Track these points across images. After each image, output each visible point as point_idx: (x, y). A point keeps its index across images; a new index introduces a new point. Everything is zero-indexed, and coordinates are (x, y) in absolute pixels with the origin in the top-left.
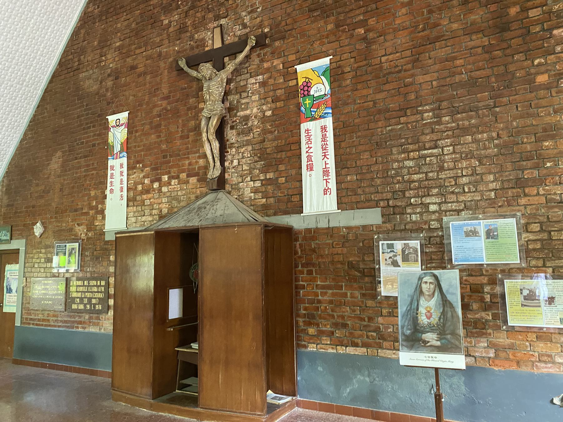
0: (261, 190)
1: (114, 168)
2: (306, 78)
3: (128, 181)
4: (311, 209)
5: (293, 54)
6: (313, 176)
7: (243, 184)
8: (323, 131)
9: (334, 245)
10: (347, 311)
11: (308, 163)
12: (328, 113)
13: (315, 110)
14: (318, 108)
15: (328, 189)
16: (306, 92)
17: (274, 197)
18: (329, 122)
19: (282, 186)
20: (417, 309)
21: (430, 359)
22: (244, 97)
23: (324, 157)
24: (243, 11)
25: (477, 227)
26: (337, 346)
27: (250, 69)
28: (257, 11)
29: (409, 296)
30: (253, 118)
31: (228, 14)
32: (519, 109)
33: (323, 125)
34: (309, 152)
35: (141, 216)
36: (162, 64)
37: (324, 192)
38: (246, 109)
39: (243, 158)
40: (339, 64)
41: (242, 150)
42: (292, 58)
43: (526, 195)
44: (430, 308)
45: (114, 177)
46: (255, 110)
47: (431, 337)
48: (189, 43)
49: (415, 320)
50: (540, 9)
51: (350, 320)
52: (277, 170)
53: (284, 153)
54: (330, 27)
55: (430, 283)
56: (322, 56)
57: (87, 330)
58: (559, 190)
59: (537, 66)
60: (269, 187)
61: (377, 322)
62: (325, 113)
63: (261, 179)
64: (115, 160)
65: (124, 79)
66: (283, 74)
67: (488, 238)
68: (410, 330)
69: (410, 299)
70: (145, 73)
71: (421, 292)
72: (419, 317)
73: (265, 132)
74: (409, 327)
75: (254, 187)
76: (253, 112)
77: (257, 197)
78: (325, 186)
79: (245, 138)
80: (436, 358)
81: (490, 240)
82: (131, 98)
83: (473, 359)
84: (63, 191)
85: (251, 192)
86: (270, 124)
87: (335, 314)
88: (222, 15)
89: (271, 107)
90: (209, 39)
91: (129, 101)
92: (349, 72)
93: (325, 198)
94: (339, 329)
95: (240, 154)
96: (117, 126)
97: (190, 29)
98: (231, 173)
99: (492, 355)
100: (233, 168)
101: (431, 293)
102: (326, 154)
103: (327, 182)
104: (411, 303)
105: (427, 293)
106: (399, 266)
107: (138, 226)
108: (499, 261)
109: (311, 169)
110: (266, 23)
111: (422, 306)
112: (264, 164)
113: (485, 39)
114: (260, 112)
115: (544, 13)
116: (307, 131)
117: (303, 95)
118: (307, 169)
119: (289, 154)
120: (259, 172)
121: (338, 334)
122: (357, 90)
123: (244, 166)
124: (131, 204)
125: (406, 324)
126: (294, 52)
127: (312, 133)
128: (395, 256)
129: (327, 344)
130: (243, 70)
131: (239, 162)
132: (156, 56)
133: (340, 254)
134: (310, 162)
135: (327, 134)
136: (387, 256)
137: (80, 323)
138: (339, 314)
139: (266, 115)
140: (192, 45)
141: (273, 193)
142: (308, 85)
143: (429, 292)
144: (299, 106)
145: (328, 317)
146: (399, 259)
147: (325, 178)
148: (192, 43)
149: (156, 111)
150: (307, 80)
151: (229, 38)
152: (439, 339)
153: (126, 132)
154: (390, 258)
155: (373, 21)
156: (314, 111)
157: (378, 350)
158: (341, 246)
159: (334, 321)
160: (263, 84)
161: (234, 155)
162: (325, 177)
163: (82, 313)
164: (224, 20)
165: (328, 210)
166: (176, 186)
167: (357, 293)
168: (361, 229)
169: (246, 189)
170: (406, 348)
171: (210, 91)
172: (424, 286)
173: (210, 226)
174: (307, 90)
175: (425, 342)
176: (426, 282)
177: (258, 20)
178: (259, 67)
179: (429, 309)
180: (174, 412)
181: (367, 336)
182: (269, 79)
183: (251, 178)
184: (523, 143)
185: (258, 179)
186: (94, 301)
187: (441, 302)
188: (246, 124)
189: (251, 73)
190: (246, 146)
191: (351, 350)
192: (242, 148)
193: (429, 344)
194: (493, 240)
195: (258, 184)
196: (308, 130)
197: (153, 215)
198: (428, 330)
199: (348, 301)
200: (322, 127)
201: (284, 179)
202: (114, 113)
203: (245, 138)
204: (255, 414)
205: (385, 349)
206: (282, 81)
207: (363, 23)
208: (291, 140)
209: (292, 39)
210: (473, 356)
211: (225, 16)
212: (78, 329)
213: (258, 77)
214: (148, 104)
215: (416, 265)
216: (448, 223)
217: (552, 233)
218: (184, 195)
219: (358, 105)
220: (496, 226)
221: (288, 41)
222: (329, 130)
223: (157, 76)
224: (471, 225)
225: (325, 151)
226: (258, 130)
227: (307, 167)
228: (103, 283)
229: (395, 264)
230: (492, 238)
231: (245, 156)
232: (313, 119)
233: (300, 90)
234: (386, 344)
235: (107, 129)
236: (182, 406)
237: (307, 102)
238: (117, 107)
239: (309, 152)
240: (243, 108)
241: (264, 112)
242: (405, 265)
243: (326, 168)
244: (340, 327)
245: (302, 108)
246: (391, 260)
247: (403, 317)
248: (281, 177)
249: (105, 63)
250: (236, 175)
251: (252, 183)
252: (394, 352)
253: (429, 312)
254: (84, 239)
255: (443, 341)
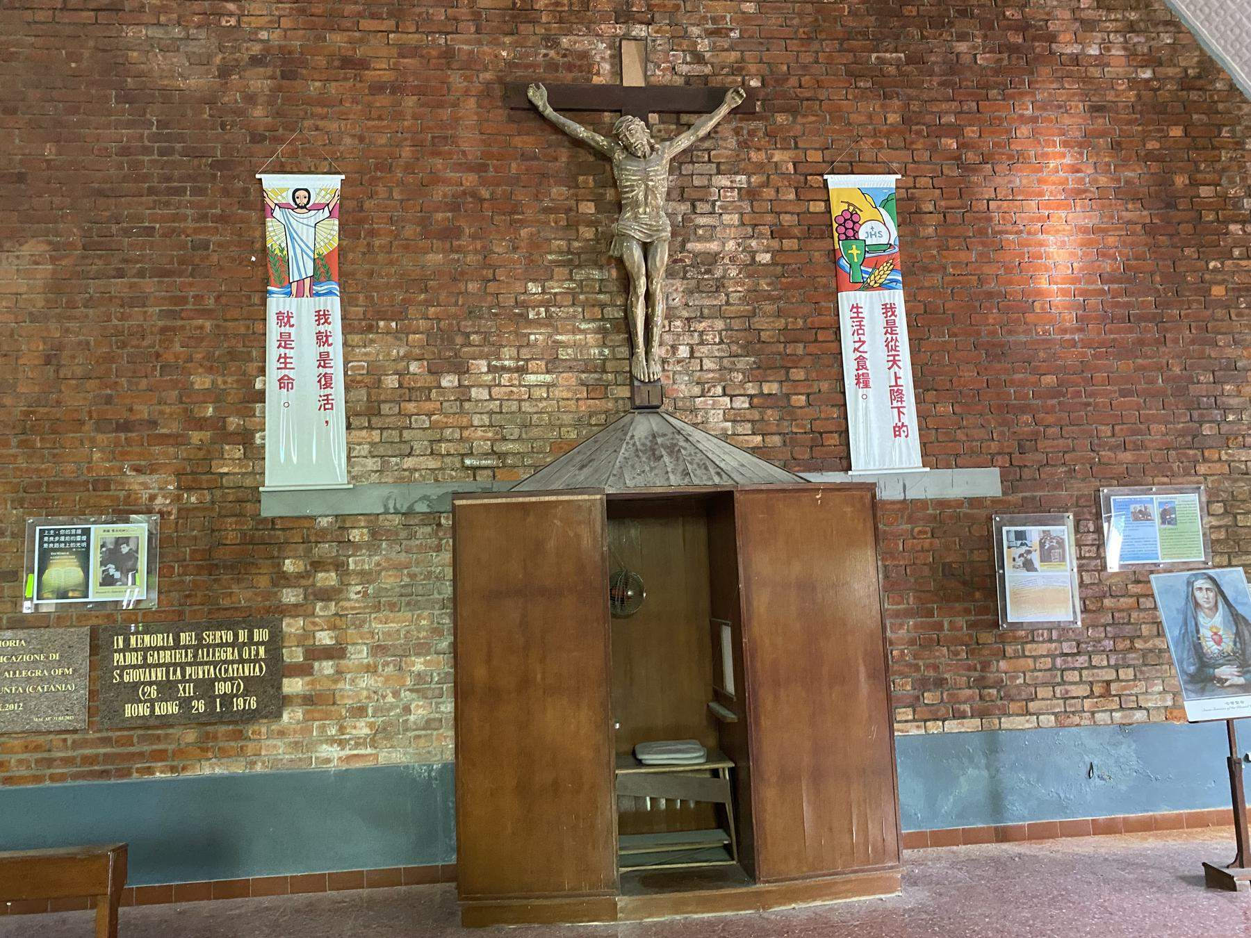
0: (749, 417)
1: (292, 321)
2: (850, 204)
3: (346, 363)
4: (867, 463)
5: (816, 149)
6: (871, 399)
7: (705, 402)
8: (889, 314)
9: (915, 534)
10: (944, 656)
11: (860, 372)
12: (897, 281)
13: (870, 270)
14: (876, 267)
15: (903, 425)
16: (850, 233)
17: (780, 434)
18: (897, 297)
19: (799, 411)
20: (1198, 631)
21: (1235, 705)
22: (702, 211)
23: (891, 363)
24: (693, 25)
25: (1149, 506)
26: (925, 721)
27: (716, 156)
28: (727, 36)
29: (1178, 610)
30: (727, 261)
31: (653, 17)
32: (1193, 331)
33: (887, 302)
34: (860, 349)
35: (402, 456)
36: (456, 79)
37: (895, 431)
38: (710, 239)
39: (702, 343)
40: (912, 193)
41: (702, 326)
42: (814, 156)
43: (1205, 460)
44: (1216, 628)
45: (294, 344)
46: (731, 245)
47: (1228, 672)
48: (544, 51)
49: (1198, 648)
50: (1212, 188)
51: (949, 671)
52: (788, 379)
53: (801, 346)
54: (893, 118)
55: (1207, 589)
56: (880, 170)
57: (188, 774)
58: (1243, 455)
59: (1212, 271)
60: (769, 412)
61: (997, 671)
62: (892, 281)
63: (749, 392)
64: (294, 299)
65: (318, 84)
66: (796, 185)
67: (1163, 523)
68: (1194, 665)
69: (1181, 617)
70: (396, 89)
71: (1197, 605)
72: (1204, 644)
73: (754, 295)
74: (1191, 660)
75: (732, 408)
76: (727, 249)
77: (740, 430)
78: (897, 421)
79: (707, 302)
80: (1242, 702)
81: (1167, 526)
82: (348, 141)
83: (1145, 712)
84: (59, 366)
85: (726, 421)
86: (768, 280)
87: (921, 663)
88: (637, 15)
89: (768, 246)
90: (602, 58)
91: (342, 148)
92: (931, 213)
93: (897, 444)
94: (929, 690)
95: (696, 334)
96: (299, 207)
97: (544, 19)
98: (671, 373)
99: (1169, 703)
100: (679, 362)
101: (1212, 604)
102: (897, 358)
103: (899, 412)
104: (1185, 623)
105: (1207, 606)
106: (1036, 570)
107: (391, 480)
108: (1178, 558)
109: (866, 385)
110: (753, 68)
111: (1203, 626)
112: (754, 362)
113: (1145, 213)
114: (743, 251)
115: (1217, 195)
116: (856, 308)
117: (843, 237)
118: (858, 383)
119: (813, 348)
120: (744, 377)
121: (929, 697)
122: (947, 249)
123: (705, 361)
124: (355, 422)
125: (1185, 656)
126: (817, 146)
127: (865, 313)
128: (1029, 552)
129: (906, 721)
130: (700, 153)
131: (692, 352)
132: (434, 53)
133: (928, 551)
134: (864, 371)
135: (897, 320)
136: (1017, 552)
137: (160, 755)
138: (928, 661)
139: (757, 259)
140: (552, 59)
141: (778, 425)
142: (851, 221)
143: (1209, 603)
144: (834, 256)
145: (906, 670)
146: (1035, 557)
147: (895, 404)
148: (552, 53)
149: (439, 193)
150: (851, 209)
151: (658, 73)
152: (1242, 674)
153: (337, 228)
154: (1021, 555)
155: (973, 132)
156: (866, 272)
157: (1000, 719)
158: (929, 535)
159: (919, 676)
160: (750, 194)
161: (680, 335)
162: (895, 402)
163: (172, 726)
164: (644, 27)
165: (904, 466)
166: (514, 389)
167: (961, 621)
168: (966, 505)
169: (713, 412)
170: (1193, 695)
171: (651, 183)
172: (1198, 594)
173: (763, 487)
174: (853, 229)
175: (1222, 681)
176: (1200, 589)
177: (733, 56)
178: (738, 155)
179: (1215, 630)
180: (690, 909)
181: (980, 696)
182: (763, 187)
183: (724, 388)
184: (1198, 382)
185: (742, 392)
186: (222, 688)
187: (1231, 619)
188: (708, 272)
189: (718, 164)
190: (709, 318)
191: (952, 726)
192: (701, 322)
193: (1227, 684)
194: (1170, 526)
195: (741, 403)
196: (857, 307)
197: (443, 456)
198: (1221, 662)
199: (946, 635)
200: (886, 305)
201: (804, 398)
202: (281, 169)
203: (707, 302)
204: (884, 869)
205: (1012, 715)
206: (792, 196)
207: (955, 131)
208: (817, 320)
209: (814, 118)
210: (1145, 709)
211: (646, 20)
212: (153, 774)
213: (738, 178)
214: (409, 168)
215: (1062, 568)
216: (1108, 498)
217: (1238, 517)
218: (541, 413)
219: (951, 278)
220: (1173, 505)
221: (804, 121)
222: (900, 313)
223: (441, 105)
224: (1140, 502)
225: (893, 353)
226: (740, 289)
227: (858, 379)
228: (261, 635)
229: (1028, 565)
230: (1169, 523)
231: (706, 340)
232: (866, 287)
233: (835, 225)
234: (1014, 707)
235: (264, 211)
236: (712, 889)
237: (855, 251)
238: (294, 154)
239: (860, 349)
240: (701, 236)
241: (753, 254)
242: (1045, 568)
243: (896, 385)
244: (932, 687)
245: (843, 262)
246: (1022, 559)
247: (1176, 646)
248: (796, 394)
249: (239, 21)
250: (687, 378)
251: (727, 399)
252: (1028, 717)
253: (1216, 634)
254: (169, 513)
255: (1248, 676)
